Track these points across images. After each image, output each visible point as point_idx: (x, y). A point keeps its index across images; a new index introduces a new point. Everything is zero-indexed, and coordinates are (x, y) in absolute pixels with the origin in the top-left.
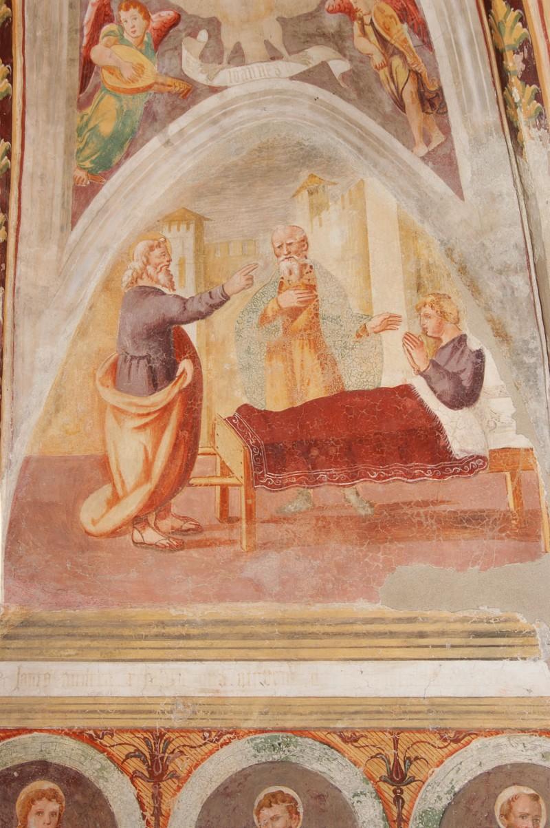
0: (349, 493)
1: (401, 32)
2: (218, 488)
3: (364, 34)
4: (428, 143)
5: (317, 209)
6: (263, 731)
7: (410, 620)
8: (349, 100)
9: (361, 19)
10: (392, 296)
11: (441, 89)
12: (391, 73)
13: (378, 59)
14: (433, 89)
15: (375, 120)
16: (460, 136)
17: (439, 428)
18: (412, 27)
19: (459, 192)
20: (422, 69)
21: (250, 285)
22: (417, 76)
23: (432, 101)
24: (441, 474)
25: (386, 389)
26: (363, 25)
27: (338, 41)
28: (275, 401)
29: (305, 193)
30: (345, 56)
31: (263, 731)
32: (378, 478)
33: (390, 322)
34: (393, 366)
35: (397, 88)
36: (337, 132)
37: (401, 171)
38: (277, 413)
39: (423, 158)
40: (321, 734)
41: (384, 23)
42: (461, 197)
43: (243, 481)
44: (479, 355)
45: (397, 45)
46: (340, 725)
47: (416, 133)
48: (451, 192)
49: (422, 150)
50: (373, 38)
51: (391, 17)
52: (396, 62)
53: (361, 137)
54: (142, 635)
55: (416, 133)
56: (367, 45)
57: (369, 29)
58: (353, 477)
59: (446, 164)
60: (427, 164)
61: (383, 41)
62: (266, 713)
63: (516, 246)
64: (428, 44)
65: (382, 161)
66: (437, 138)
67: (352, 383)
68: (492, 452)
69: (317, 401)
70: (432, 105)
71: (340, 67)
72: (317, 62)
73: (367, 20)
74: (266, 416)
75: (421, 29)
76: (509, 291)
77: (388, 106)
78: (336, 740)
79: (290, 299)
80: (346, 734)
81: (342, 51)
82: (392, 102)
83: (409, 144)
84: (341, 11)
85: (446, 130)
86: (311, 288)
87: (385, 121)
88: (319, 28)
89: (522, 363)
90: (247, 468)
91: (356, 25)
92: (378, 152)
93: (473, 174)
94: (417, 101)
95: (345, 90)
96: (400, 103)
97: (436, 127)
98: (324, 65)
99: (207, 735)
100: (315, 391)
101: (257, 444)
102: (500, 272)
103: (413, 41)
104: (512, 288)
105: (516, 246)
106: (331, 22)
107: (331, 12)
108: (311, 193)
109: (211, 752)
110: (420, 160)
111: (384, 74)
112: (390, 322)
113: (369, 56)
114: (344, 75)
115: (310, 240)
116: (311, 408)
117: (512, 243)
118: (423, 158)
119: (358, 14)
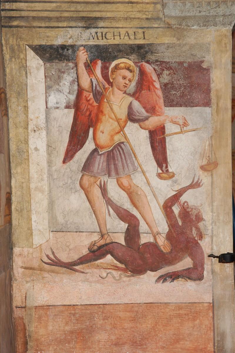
54: (170, 103)
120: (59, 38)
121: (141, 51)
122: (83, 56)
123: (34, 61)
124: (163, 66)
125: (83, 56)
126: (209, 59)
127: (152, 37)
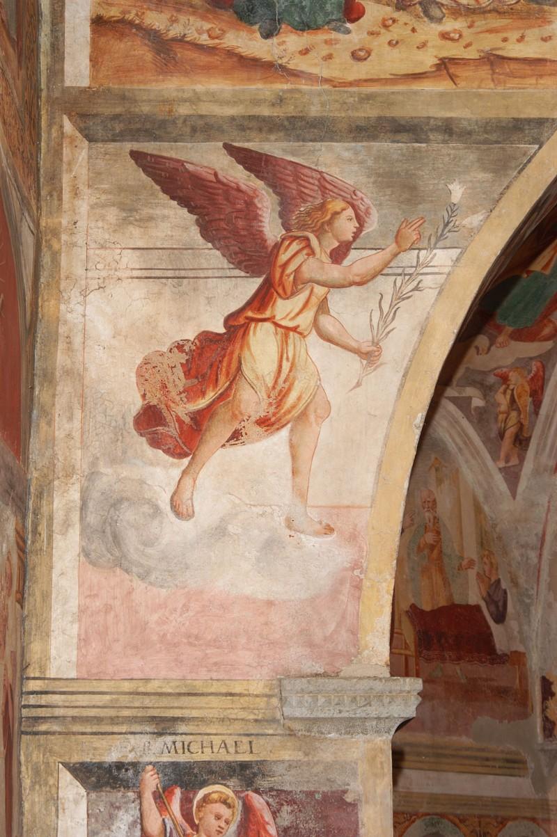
0: (458, 668)
1: (526, 401)
2: (404, 657)
3: (505, 393)
4: (507, 461)
5: (440, 481)
6: (429, 814)
7: (483, 750)
8: (470, 421)
9: (509, 385)
10: (472, 551)
11: (530, 437)
12: (507, 418)
13: (503, 408)
14: (525, 435)
15: (480, 437)
16: (528, 466)
17: (491, 634)
18: (534, 401)
19: (514, 495)
20: (526, 423)
21: (413, 524)
22: (521, 426)
23: (521, 441)
24: (492, 662)
25: (470, 605)
26: (507, 388)
27: (487, 390)
28: (427, 607)
29: (433, 469)
30: (485, 398)
31: (429, 814)
32: (468, 661)
33: (471, 563)
34: (474, 596)
35: (505, 427)
36: (450, 435)
37: (482, 471)
38: (427, 612)
39: (500, 469)
40: (451, 817)
41: (520, 393)
42: (514, 498)
43: (414, 654)
44: (505, 592)
45: (520, 406)
46: (459, 812)
47: (502, 454)
48: (508, 492)
49: (502, 464)
50: (508, 397)
51: (526, 392)
52: (514, 414)
53: (465, 443)
55: (502, 454)
56: (503, 400)
57: (509, 392)
58: (459, 659)
59: (512, 477)
60: (501, 473)
61: (513, 401)
62: (429, 803)
63: (536, 535)
64: (537, 413)
65: (473, 462)
66: (514, 461)
67: (458, 600)
68: (511, 652)
69: (443, 607)
70: (520, 444)
71: (478, 402)
72: (467, 395)
73: (511, 387)
74: (422, 612)
75: (537, 404)
76: (525, 559)
77: (493, 434)
78: (457, 821)
79: (430, 538)
80: (351, 808)
81: (485, 396)
82: (497, 432)
83: (495, 458)
84: (500, 377)
85: (522, 459)
86: (438, 533)
87: (487, 441)
88: (483, 380)
89: (524, 601)
90: (415, 646)
91: (504, 386)
92: (472, 455)
93: (527, 487)
94: (513, 438)
95: (472, 415)
96: (501, 435)
97: (516, 456)
98: (470, 398)
99: (405, 816)
100: (442, 602)
101: (419, 630)
102: (522, 546)
103: (530, 408)
104: (527, 559)
105: (536, 535)
106: (492, 379)
107: (494, 375)
108: (437, 470)
109: (407, 827)
110: (497, 470)
111: (501, 417)
112: (471, 563)
113: (499, 405)
114: (477, 408)
115: (437, 500)
116: (441, 610)
117: (535, 532)
118: (500, 469)
119: (508, 383)
120: (113, 752)
121: (246, 774)
122: (151, 781)
123: (71, 790)
124: (281, 797)
125: (151, 781)
126: (355, 789)
127: (262, 751)
